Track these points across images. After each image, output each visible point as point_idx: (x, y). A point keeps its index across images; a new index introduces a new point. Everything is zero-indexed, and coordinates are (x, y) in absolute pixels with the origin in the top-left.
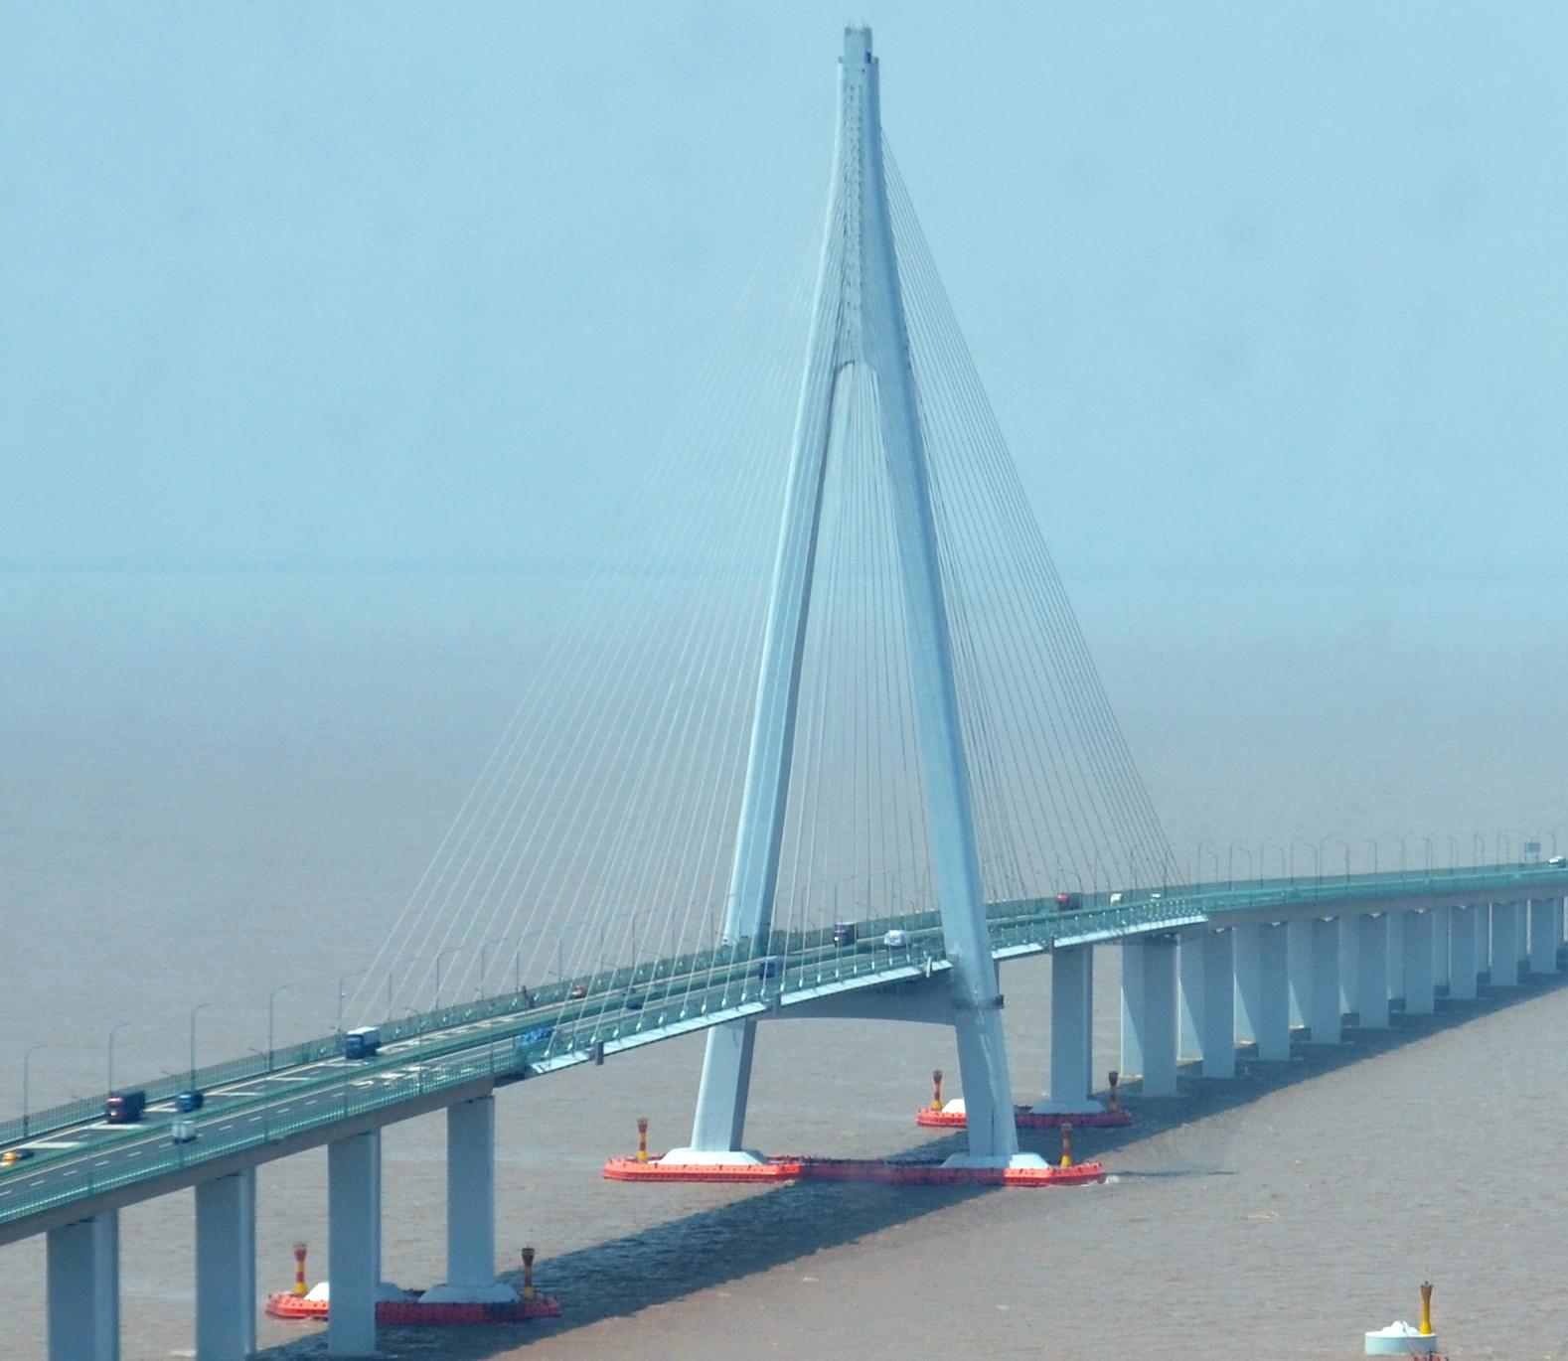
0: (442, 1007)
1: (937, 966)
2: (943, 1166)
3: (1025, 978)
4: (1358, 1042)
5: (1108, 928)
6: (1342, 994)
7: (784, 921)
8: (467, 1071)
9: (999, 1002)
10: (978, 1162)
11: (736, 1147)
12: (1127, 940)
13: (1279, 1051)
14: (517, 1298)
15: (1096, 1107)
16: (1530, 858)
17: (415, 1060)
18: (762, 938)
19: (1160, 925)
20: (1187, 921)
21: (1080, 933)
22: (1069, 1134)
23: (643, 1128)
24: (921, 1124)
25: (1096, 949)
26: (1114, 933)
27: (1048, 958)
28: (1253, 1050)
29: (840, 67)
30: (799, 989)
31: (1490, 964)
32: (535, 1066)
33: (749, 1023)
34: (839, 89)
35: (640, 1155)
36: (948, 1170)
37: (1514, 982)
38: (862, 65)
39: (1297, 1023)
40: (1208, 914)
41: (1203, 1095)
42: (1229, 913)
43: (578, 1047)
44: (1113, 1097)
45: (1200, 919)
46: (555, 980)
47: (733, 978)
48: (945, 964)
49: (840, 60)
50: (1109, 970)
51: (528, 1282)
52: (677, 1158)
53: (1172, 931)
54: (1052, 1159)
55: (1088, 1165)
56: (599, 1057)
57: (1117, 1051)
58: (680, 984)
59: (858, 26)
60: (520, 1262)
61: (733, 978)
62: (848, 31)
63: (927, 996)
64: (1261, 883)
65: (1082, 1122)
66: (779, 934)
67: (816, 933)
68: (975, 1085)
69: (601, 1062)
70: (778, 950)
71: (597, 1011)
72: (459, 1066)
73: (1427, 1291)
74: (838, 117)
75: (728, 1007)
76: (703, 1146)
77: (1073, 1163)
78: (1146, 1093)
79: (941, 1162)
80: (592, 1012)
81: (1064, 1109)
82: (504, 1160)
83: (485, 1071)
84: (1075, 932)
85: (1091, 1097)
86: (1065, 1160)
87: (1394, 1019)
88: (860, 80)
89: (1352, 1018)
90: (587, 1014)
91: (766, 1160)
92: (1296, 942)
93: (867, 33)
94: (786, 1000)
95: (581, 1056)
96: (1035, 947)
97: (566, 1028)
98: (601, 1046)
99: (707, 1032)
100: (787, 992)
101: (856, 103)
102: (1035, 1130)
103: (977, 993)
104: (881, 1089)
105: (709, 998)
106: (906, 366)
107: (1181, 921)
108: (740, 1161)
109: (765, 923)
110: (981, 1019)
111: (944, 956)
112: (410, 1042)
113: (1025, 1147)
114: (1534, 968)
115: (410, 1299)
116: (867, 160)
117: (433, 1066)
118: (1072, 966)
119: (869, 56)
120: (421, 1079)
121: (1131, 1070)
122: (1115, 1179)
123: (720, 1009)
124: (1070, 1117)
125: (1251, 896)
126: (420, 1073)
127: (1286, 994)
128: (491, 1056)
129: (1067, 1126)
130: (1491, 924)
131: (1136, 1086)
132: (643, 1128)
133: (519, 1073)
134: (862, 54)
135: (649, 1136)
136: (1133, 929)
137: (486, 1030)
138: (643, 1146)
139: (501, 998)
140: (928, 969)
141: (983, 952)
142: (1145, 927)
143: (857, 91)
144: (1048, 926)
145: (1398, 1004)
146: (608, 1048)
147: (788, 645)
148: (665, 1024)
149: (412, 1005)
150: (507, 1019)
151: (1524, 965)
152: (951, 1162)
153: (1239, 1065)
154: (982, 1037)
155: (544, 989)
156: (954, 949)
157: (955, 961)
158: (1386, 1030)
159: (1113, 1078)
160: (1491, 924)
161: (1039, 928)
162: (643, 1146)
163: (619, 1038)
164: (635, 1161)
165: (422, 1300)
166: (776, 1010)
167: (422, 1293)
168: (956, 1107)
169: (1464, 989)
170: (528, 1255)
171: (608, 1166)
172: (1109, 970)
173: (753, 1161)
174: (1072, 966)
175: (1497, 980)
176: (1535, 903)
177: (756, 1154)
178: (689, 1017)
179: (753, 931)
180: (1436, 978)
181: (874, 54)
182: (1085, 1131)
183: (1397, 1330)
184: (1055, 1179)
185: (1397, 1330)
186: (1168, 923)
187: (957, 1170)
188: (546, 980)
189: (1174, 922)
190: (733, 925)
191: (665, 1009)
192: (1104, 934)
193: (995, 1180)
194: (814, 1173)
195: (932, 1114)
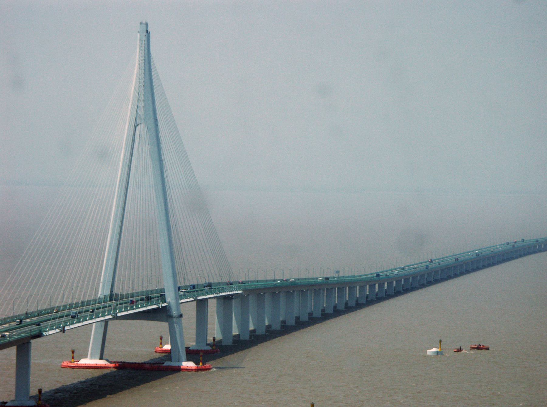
0: (15, 314)
1: (163, 305)
2: (164, 365)
3: (188, 308)
4: (286, 329)
5: (213, 294)
6: (266, 318)
7: (115, 291)
8: (23, 335)
9: (181, 316)
10: (174, 364)
11: (101, 358)
12: (218, 298)
13: (246, 337)
14: (36, 404)
15: (209, 348)
16: (337, 275)
17: (7, 331)
18: (111, 295)
19: (229, 293)
20: (236, 292)
21: (205, 295)
22: (202, 356)
23: (73, 352)
24: (156, 352)
25: (209, 300)
26: (215, 295)
27: (195, 303)
28: (238, 336)
29: (138, 34)
30: (122, 312)
31: (347, 299)
32: (44, 333)
33: (106, 321)
34: (138, 42)
35: (73, 360)
36: (165, 366)
37: (320, 316)
38: (145, 34)
39: (251, 328)
40: (243, 290)
41: (239, 345)
42: (249, 290)
43: (57, 328)
44: (214, 345)
45: (241, 292)
46: (49, 307)
47: (103, 308)
48: (166, 304)
49: (139, 32)
50: (213, 307)
51: (40, 399)
52: (83, 362)
53: (232, 295)
54: (197, 363)
55: (208, 365)
56: (63, 331)
57: (215, 332)
58: (98, 307)
59: (144, 22)
60: (37, 393)
61: (103, 308)
62: (141, 23)
63: (161, 314)
64: (258, 281)
65: (206, 352)
66: (117, 295)
67: (128, 294)
68: (174, 343)
69: (64, 332)
70: (116, 300)
71: (63, 317)
72: (21, 333)
73: (441, 341)
74: (138, 50)
75: (101, 316)
76: (91, 358)
77: (203, 365)
78: (224, 344)
79: (163, 363)
80: (61, 317)
81: (200, 348)
82: (37, 362)
83: (29, 334)
84: (203, 295)
85: (208, 345)
86: (201, 364)
87: (282, 327)
88: (144, 38)
89: (269, 327)
90: (60, 317)
91: (111, 362)
92: (268, 298)
93: (147, 24)
94: (119, 315)
95: (58, 330)
96: (192, 299)
97: (80, 315)
98: (64, 327)
99: (94, 324)
100: (119, 312)
101: (143, 45)
102: (191, 355)
103: (175, 313)
104: (142, 342)
105: (108, 311)
106: (157, 125)
107: (234, 292)
108: (102, 363)
109: (112, 291)
110: (175, 320)
111: (165, 302)
112: (5, 326)
113: (188, 360)
114: (349, 305)
115: (3, 404)
116: (147, 63)
117: (12, 333)
118: (202, 305)
119: (147, 32)
120: (9, 337)
121: (219, 337)
122: (215, 369)
123: (99, 317)
124: (202, 351)
125: (255, 285)
126: (9, 335)
127: (248, 319)
128: (31, 330)
129: (201, 353)
130: (336, 295)
131: (221, 341)
132: (73, 352)
133: (39, 335)
134: (145, 31)
135: (75, 355)
136: (221, 294)
137: (6, 327)
138: (73, 358)
139: (19, 315)
140: (160, 305)
141: (177, 300)
142: (224, 294)
143: (144, 42)
144: (196, 293)
145: (284, 322)
146: (66, 328)
147: (120, 209)
148: (83, 321)
149: (6, 313)
150: (35, 319)
151: (346, 304)
152: (167, 364)
153: (251, 336)
154: (175, 325)
155: (45, 310)
156: (168, 300)
157: (169, 303)
158: (265, 335)
159: (214, 339)
160: (336, 295)
161: (193, 293)
162: (73, 358)
163: (69, 325)
164: (71, 362)
165: (7, 405)
166: (116, 318)
167: (6, 403)
168: (167, 347)
169: (317, 314)
170: (40, 391)
171: (62, 364)
172: (213, 307)
173: (106, 363)
174: (202, 305)
175: (327, 311)
176: (338, 288)
177: (107, 360)
178: (90, 319)
179: (108, 293)
180: (296, 314)
181: (149, 31)
182: (208, 355)
183: (434, 350)
184: (197, 370)
185: (434, 350)
186: (231, 293)
187: (168, 366)
188: (45, 307)
189: (233, 293)
190: (103, 291)
191: (83, 317)
192: (212, 296)
193: (178, 369)
194: (122, 366)
195: (159, 349)
